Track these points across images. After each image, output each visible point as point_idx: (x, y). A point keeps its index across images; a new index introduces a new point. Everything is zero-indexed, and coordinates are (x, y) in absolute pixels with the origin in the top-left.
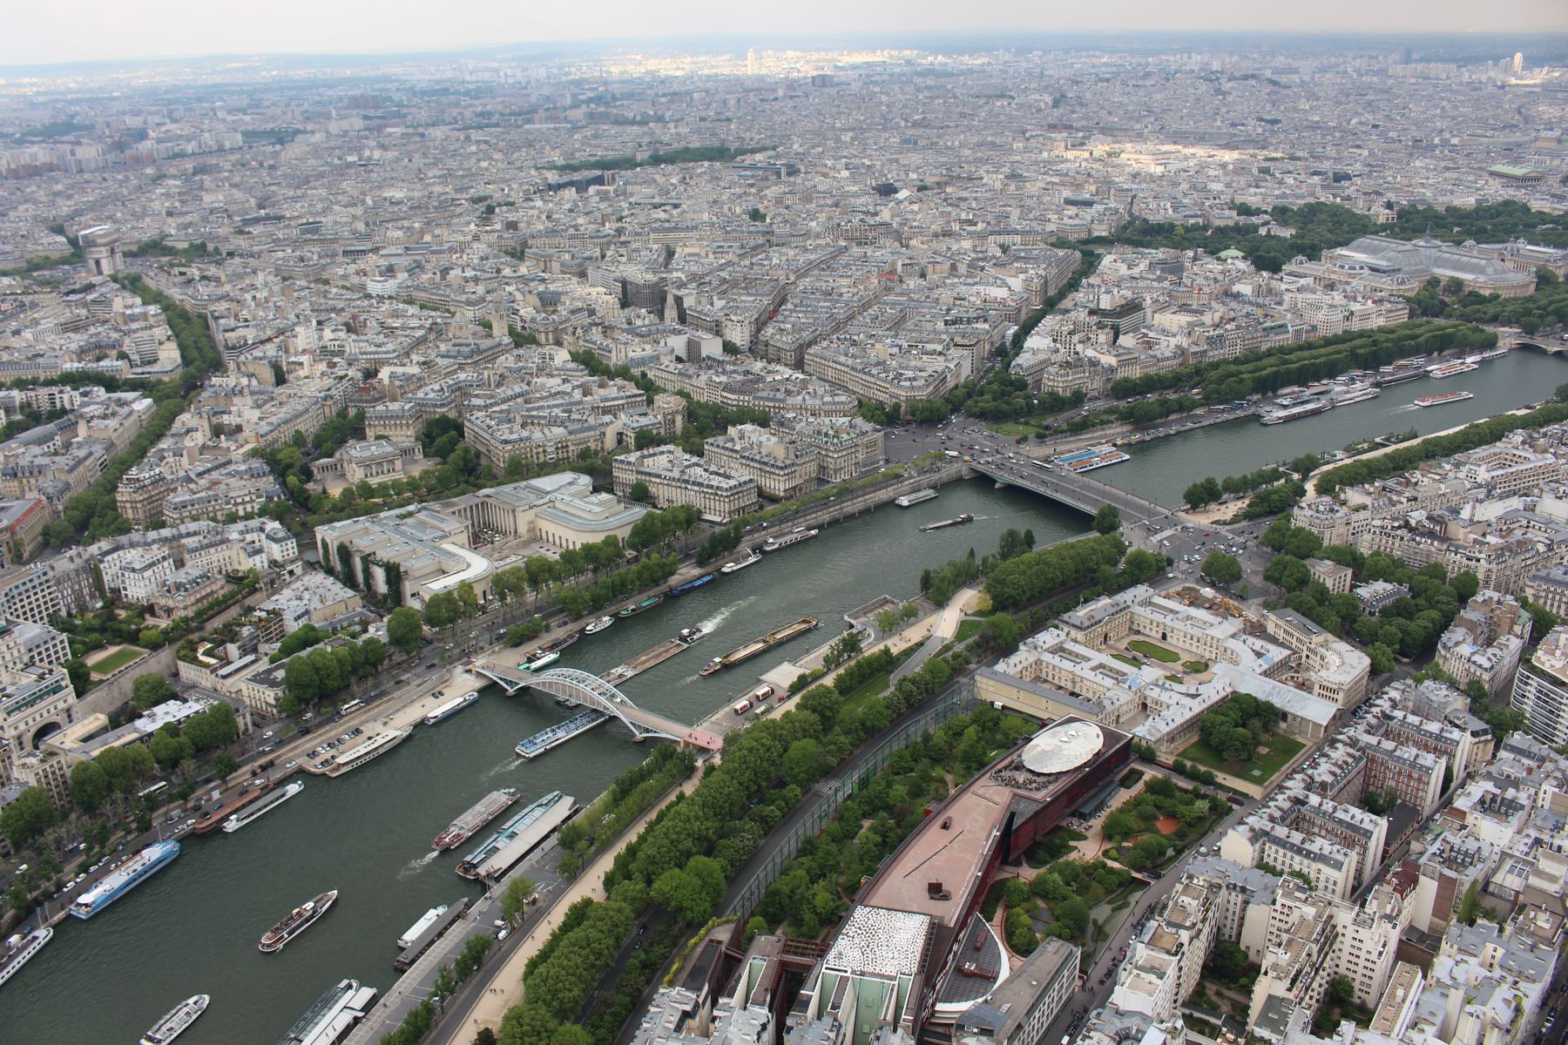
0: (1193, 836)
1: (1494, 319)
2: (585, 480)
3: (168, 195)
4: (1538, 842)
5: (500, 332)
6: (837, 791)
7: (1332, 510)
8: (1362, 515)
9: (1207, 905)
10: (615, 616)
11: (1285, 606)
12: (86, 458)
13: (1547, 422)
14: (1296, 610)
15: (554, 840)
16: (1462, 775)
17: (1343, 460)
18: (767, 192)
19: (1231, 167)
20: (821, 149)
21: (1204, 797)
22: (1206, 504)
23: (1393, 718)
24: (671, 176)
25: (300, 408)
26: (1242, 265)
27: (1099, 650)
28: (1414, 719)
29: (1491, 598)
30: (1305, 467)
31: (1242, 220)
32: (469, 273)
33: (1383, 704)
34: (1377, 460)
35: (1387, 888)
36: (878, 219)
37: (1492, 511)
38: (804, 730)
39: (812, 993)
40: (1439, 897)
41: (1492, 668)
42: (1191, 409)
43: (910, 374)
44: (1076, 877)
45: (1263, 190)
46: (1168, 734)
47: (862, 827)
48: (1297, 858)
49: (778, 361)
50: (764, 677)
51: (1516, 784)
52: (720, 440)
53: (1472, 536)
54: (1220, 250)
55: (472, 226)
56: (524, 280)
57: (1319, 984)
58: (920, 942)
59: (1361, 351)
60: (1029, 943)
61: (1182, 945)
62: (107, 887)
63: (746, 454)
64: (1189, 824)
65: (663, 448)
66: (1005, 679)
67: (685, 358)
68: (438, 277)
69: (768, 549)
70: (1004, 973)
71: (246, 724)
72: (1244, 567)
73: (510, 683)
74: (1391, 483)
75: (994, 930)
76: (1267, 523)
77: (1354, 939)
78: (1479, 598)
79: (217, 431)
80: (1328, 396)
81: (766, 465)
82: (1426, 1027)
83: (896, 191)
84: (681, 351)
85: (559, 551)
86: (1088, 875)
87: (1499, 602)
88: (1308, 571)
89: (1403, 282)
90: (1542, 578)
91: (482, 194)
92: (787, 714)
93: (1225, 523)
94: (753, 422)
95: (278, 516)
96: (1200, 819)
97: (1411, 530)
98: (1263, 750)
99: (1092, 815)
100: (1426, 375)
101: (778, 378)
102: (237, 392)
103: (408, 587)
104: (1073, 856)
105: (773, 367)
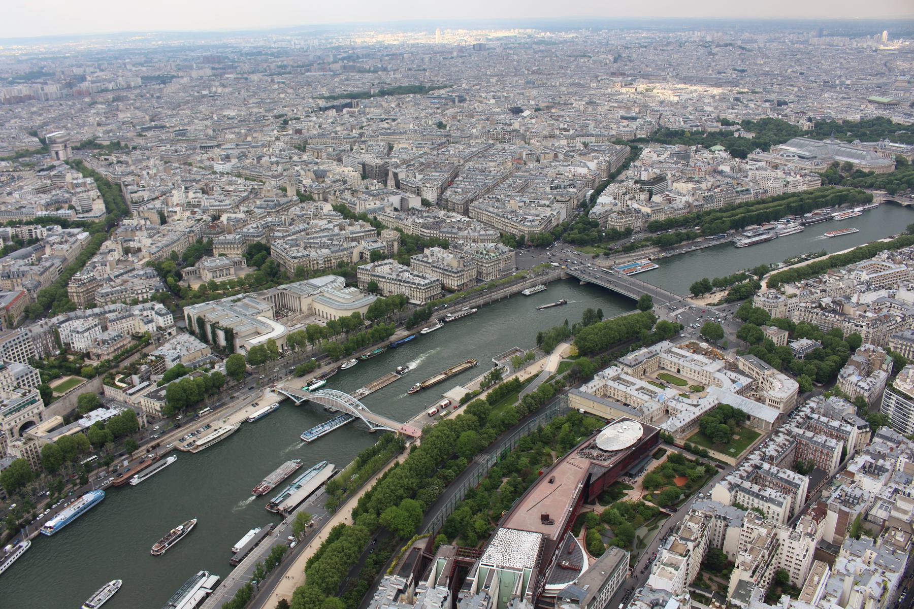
0: (695, 487)
1: (871, 186)
2: (341, 280)
3: (98, 114)
4: (896, 491)
5: (291, 193)
6: (488, 461)
7: (776, 297)
8: (794, 300)
9: (703, 527)
10: (358, 359)
11: (749, 353)
12: (50, 267)
13: (902, 246)
14: (756, 355)
15: (323, 489)
16: (852, 451)
17: (783, 268)
18: (447, 112)
19: (718, 97)
20: (478, 87)
21: (702, 464)
22: (703, 293)
23: (812, 418)
24: (391, 102)
25: (175, 238)
26: (724, 155)
27: (641, 379)
28: (824, 419)
29: (869, 349)
30: (761, 272)
31: (724, 128)
32: (274, 159)
33: (806, 410)
34: (803, 268)
35: (809, 518)
36: (512, 127)
37: (870, 298)
38: (469, 426)
39: (473, 579)
40: (839, 523)
41: (870, 389)
42: (694, 239)
43: (530, 218)
44: (627, 511)
45: (736, 111)
46: (681, 428)
47: (502, 482)
48: (756, 500)
49: (454, 210)
50: (445, 395)
51: (884, 457)
52: (420, 256)
53: (858, 312)
54: (711, 146)
55: (275, 132)
56: (306, 163)
57: (769, 573)
58: (537, 549)
59: (793, 205)
60: (600, 550)
61: (689, 551)
62: (62, 517)
63: (435, 265)
64: (693, 480)
65: (387, 261)
66: (586, 396)
67: (399, 208)
68: (255, 161)
69: (447, 320)
70: (585, 567)
71: (143, 422)
72: (725, 330)
73: (297, 398)
74: (811, 281)
75: (580, 542)
76: (738, 305)
77: (789, 547)
78: (862, 349)
79: (127, 251)
80: (774, 231)
81: (446, 271)
82: (831, 599)
83: (522, 111)
84: (397, 204)
85: (326, 321)
86: (634, 510)
87: (874, 351)
88: (763, 333)
89: (818, 165)
90: (899, 337)
91: (281, 113)
92: (459, 416)
93: (714, 305)
94: (439, 246)
95: (162, 301)
96: (700, 477)
97: (823, 309)
98: (736, 437)
99: (637, 475)
100: (831, 218)
101: (453, 220)
102: (138, 228)
103: (238, 342)
104: (625, 499)
105: (451, 214)
